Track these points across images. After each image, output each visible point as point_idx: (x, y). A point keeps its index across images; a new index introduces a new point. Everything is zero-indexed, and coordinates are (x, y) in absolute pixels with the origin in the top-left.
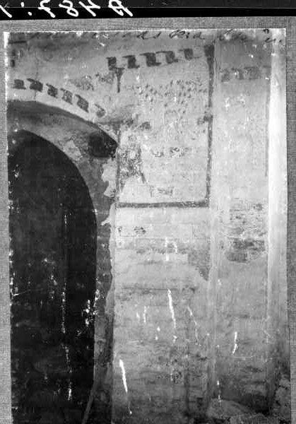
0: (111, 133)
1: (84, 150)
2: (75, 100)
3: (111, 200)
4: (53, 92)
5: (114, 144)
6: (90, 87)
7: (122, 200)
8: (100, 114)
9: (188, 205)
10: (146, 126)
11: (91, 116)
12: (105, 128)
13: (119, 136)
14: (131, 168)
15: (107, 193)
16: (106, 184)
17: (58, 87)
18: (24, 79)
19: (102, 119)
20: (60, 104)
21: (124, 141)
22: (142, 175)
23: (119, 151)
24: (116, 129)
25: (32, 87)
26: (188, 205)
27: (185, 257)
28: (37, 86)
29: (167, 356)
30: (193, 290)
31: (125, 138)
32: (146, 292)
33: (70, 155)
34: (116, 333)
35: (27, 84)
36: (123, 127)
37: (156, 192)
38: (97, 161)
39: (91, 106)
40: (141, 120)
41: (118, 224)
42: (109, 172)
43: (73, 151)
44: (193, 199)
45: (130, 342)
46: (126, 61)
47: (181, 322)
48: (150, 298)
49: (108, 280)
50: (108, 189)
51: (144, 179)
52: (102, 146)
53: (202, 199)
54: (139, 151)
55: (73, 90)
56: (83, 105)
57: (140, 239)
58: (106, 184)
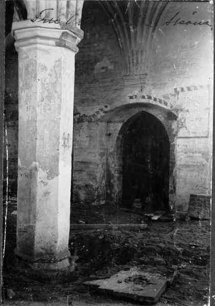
0: (175, 113)
1: (165, 118)
2: (163, 102)
3: (175, 135)
4: (155, 100)
5: (177, 117)
6: (168, 98)
7: (179, 136)
8: (171, 107)
9: (202, 137)
10: (188, 111)
11: (168, 108)
12: (173, 112)
13: (178, 115)
14: (182, 125)
15: (174, 133)
16: (173, 129)
17: (157, 98)
18: (145, 95)
19: (172, 109)
20: (158, 103)
21: (180, 116)
22: (186, 127)
23: (178, 119)
24: (177, 112)
25: (148, 98)
26: (202, 137)
27: (200, 155)
28: (150, 98)
29: (195, 188)
30: (203, 165)
31: (180, 115)
32: (188, 166)
33: (160, 119)
34: (177, 180)
35: (146, 97)
36: (179, 112)
37: (191, 133)
38: (170, 121)
39: (169, 104)
40: (186, 109)
41: (178, 144)
42: (174, 125)
43: (161, 118)
44: (203, 135)
45: (179, 249)
46: (181, 89)
47: (35, 91)
48: (188, 169)
49: (174, 163)
50: (174, 131)
51: (187, 129)
52: (171, 116)
53: (205, 135)
54: (185, 120)
55: (162, 99)
56: (166, 104)
57: (171, 231)
58: (173, 129)
